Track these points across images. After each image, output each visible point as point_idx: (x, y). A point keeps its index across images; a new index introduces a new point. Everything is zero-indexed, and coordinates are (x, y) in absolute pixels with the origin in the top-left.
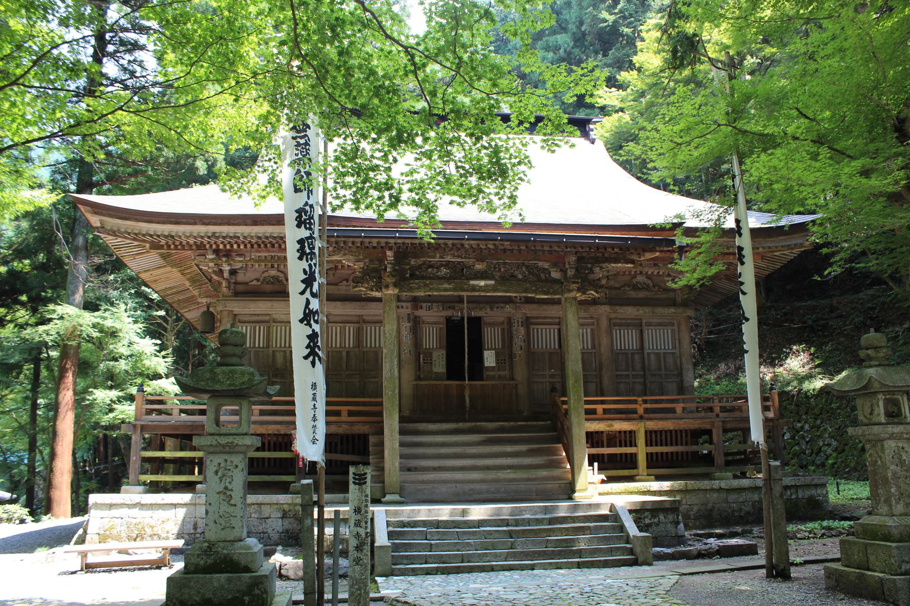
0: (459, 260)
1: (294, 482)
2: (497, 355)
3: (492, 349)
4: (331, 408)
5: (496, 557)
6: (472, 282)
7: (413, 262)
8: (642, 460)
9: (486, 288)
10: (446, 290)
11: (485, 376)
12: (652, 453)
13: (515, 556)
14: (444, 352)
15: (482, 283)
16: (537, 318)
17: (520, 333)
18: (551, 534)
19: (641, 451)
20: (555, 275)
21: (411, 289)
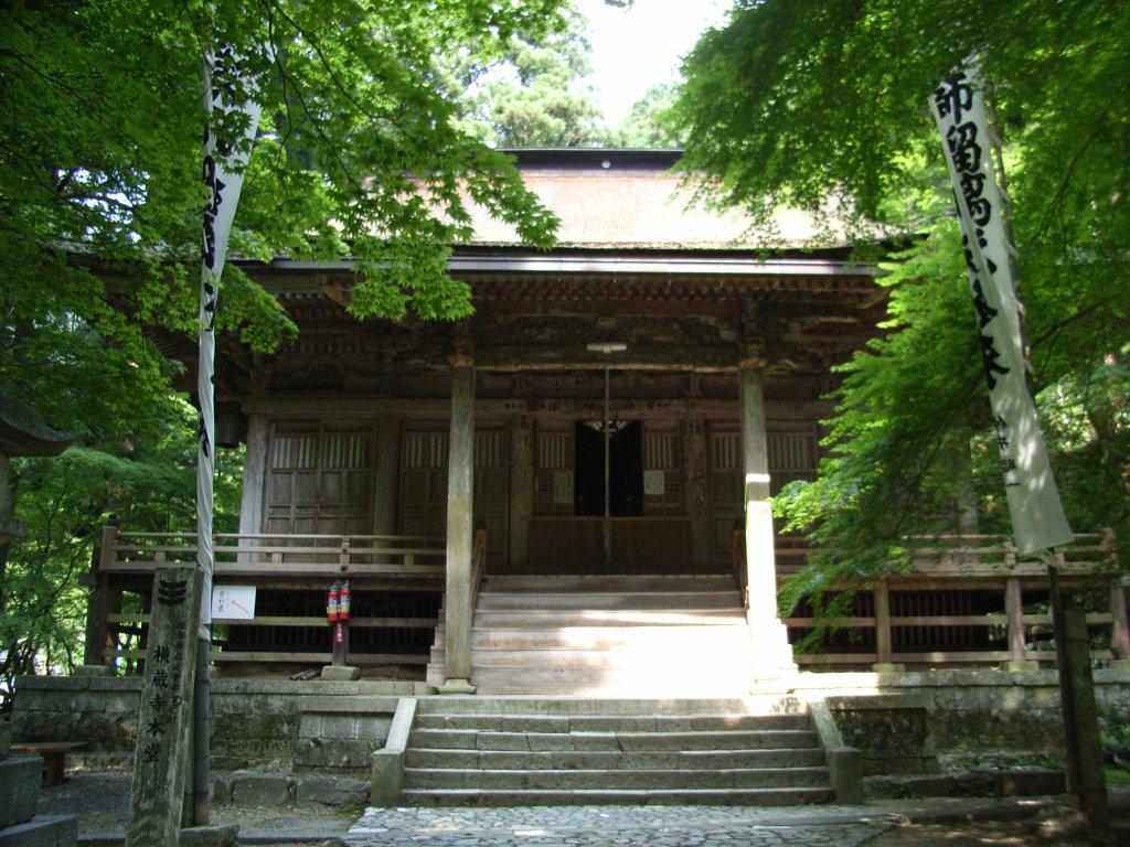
0: (572, 315)
1: (330, 664)
2: (667, 477)
3: (657, 468)
4: (903, 631)
5: (584, 781)
6: (592, 348)
7: (501, 320)
8: (884, 638)
9: (614, 357)
10: (552, 361)
11: (645, 509)
12: (899, 628)
13: (620, 781)
14: (572, 474)
15: (607, 349)
16: (723, 420)
17: (696, 443)
18: (457, 744)
19: (884, 625)
20: (727, 335)
21: (496, 362)
